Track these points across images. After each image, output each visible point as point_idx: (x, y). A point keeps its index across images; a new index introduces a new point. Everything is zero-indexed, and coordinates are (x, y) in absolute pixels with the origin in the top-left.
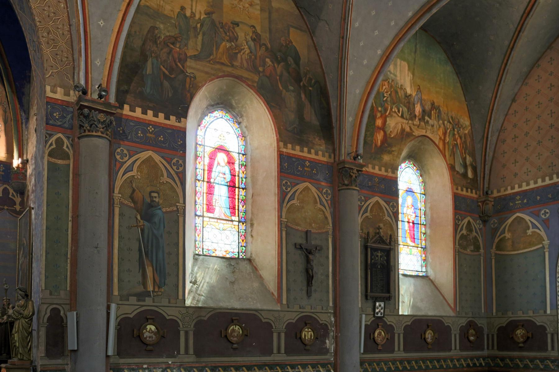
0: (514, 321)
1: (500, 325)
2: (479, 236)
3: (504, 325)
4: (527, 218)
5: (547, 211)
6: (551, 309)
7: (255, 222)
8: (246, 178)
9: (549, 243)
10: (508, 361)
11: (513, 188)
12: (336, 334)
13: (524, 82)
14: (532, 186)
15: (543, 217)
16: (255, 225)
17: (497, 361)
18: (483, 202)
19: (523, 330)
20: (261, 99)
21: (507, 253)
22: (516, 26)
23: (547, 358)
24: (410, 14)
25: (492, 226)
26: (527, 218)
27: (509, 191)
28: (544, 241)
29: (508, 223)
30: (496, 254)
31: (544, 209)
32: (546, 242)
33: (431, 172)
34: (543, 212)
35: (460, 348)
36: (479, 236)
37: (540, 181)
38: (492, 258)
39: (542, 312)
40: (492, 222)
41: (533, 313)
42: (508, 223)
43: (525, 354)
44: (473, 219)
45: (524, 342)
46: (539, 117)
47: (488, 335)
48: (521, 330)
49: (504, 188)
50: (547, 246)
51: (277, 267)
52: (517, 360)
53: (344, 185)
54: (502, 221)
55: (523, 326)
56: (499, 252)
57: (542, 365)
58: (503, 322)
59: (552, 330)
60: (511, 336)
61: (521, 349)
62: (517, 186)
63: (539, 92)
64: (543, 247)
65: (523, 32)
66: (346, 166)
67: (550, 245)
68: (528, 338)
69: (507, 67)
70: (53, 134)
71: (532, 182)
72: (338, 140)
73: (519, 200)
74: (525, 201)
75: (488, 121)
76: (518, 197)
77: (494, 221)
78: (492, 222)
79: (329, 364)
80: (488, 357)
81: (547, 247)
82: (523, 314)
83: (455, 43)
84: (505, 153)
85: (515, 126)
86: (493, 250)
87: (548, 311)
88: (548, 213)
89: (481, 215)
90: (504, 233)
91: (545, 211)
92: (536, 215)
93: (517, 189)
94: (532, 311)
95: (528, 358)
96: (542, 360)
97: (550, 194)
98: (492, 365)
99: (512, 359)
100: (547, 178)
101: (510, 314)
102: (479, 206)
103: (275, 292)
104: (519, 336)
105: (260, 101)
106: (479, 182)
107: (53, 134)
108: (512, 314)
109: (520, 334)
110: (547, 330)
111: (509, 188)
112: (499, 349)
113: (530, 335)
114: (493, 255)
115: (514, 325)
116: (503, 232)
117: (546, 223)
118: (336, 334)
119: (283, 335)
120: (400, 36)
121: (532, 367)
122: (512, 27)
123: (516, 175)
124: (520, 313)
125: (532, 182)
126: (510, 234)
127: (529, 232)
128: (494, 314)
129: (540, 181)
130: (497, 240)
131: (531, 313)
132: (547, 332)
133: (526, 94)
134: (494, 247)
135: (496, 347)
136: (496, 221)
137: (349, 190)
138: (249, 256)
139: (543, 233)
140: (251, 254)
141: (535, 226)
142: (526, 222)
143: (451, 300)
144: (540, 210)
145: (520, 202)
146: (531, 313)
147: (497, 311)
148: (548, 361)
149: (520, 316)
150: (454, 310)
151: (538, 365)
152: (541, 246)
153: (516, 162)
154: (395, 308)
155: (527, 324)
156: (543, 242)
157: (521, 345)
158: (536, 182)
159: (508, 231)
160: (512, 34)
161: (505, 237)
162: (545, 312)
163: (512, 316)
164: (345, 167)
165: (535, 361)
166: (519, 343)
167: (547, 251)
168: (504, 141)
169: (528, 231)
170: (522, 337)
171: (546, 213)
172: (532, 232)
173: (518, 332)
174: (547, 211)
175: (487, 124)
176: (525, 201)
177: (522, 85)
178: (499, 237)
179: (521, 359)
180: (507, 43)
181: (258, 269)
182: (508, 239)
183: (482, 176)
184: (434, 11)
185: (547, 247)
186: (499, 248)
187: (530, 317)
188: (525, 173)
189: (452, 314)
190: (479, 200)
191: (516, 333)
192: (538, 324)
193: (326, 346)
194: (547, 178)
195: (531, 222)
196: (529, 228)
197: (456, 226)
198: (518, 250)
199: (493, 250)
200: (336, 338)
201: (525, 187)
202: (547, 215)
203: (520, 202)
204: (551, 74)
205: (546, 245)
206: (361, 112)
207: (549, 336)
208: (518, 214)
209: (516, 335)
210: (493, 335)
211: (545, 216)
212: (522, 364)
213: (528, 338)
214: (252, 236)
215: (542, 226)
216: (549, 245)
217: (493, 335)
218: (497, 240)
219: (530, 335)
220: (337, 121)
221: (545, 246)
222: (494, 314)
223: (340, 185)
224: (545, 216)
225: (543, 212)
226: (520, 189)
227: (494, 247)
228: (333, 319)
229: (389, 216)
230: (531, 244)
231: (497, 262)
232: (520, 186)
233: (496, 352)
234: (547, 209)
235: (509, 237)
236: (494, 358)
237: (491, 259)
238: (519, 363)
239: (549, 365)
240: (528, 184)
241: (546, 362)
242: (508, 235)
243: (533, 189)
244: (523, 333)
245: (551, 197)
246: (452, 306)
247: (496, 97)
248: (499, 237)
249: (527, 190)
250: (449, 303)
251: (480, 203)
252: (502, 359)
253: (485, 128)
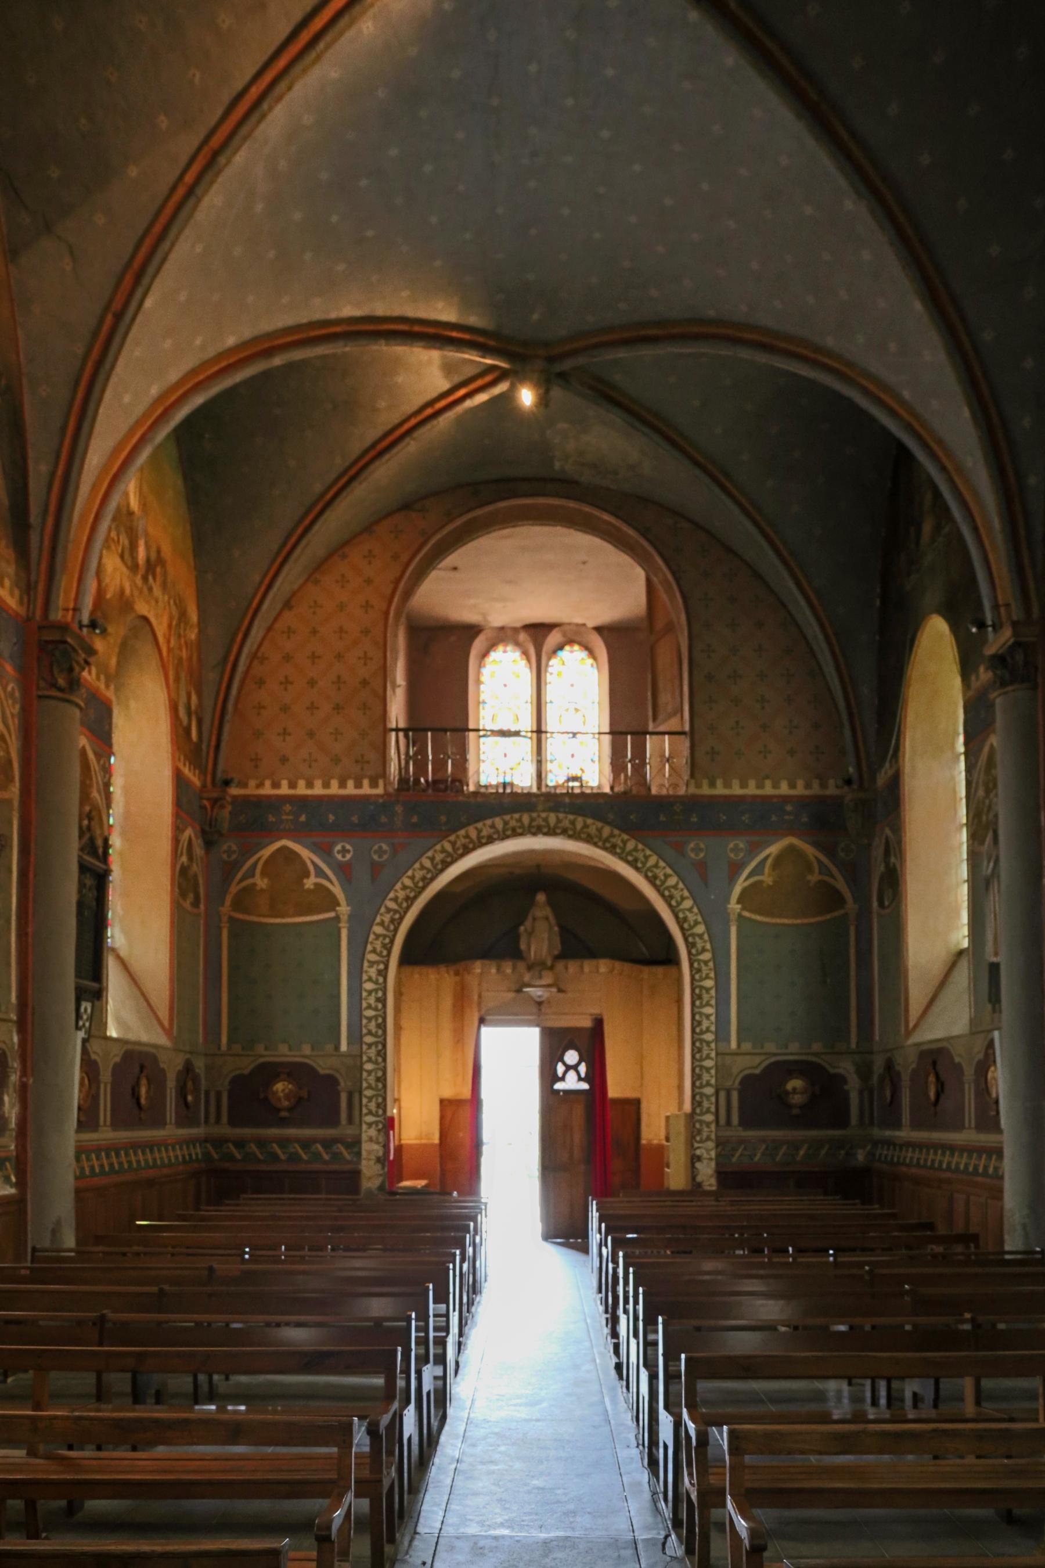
0: (269, 1063)
1: (238, 1072)
3: (246, 1072)
4: (305, 853)
5: (348, 847)
6: (349, 1044)
9: (349, 912)
10: (253, 1147)
11: (276, 785)
13: (310, 575)
14: (318, 790)
15: (339, 857)
17: (228, 1148)
18: (215, 802)
19: (290, 1083)
21: (255, 919)
22: (347, 464)
24: (231, 341)
25: (225, 856)
26: (305, 853)
27: (267, 790)
28: (339, 905)
29: (259, 859)
30: (232, 920)
31: (343, 841)
32: (344, 909)
33: (133, 704)
34: (339, 847)
37: (334, 783)
38: (223, 925)
39: (329, 1047)
40: (225, 847)
41: (313, 1049)
42: (259, 859)
43: (292, 1132)
44: (732, 879)
45: (290, 1109)
46: (339, 657)
47: (207, 1093)
48: (286, 1083)
49: (257, 782)
52: (274, 1145)
53: (54, 685)
54: (249, 850)
55: (289, 1074)
56: (241, 916)
57: (327, 1153)
58: (246, 1065)
59: (349, 1084)
60: (262, 1096)
61: (283, 1123)
62: (285, 783)
63: (341, 607)
64: (337, 919)
65: (360, 484)
66: (69, 640)
67: (351, 917)
68: (300, 1099)
69: (309, 536)
71: (318, 783)
72: (44, 566)
73: (288, 814)
74: (303, 818)
75: (244, 628)
76: (288, 807)
77: (229, 846)
78: (225, 847)
79: (7, 1159)
80: (206, 1141)
81: (344, 918)
82: (290, 1049)
83: (207, 436)
84: (261, 707)
85: (287, 658)
86: (226, 909)
87: (344, 1047)
88: (348, 851)
89: (207, 829)
90: (253, 876)
91: (343, 847)
92: (324, 851)
93: (284, 790)
94: (309, 1045)
95: (298, 1140)
96: (328, 1144)
97: (356, 816)
98: (216, 1156)
99: (262, 1143)
100: (350, 783)
101: (260, 1049)
102: (203, 808)
104: (281, 1095)
106: (204, 754)
108: (266, 1049)
109: (283, 1090)
111: (268, 783)
112: (233, 1122)
113: (305, 1095)
114: (225, 919)
115: (270, 1072)
116: (251, 873)
117: (344, 871)
120: (201, 377)
121: (305, 1157)
122: (339, 463)
123: (284, 760)
124: (283, 1049)
125: (318, 783)
127: (309, 883)
129: (334, 783)
130: (234, 889)
131: (307, 1050)
133: (315, 602)
135: (225, 1119)
136: (234, 848)
137: (66, 705)
139: (337, 890)
141: (320, 873)
142: (303, 863)
143: (164, 1013)
144: (334, 844)
145: (291, 817)
146: (307, 1050)
147: (230, 1041)
148: (339, 1145)
149: (284, 1054)
150: (168, 1032)
151: (320, 1154)
152: (332, 914)
153: (285, 733)
154: (102, 1021)
155: (298, 1072)
156: (338, 908)
157: (284, 1114)
160: (333, 476)
161: (254, 885)
162: (337, 1047)
164: (65, 642)
166: (279, 1110)
167: (344, 927)
168: (261, 682)
169: (305, 881)
170: (287, 1097)
171: (344, 851)
172: (316, 884)
173: (279, 1086)
174: (348, 847)
175: (240, 636)
176: (303, 818)
177: (307, 580)
179: (283, 1142)
180: (318, 488)
182: (262, 890)
183: (213, 743)
184: (277, 361)
185: (344, 918)
186: (238, 904)
188: (305, 760)
189: (163, 1040)
190: (205, 795)
191: (275, 1088)
192: (322, 1072)
193: (4, 1112)
194: (350, 783)
195: (313, 862)
196: (307, 874)
197: (176, 841)
198: (283, 917)
199: (226, 909)
200: (23, 1090)
201: (302, 790)
202: (348, 856)
203: (291, 817)
204: (369, 581)
205: (344, 915)
206: (92, 516)
207: (344, 1097)
209: (275, 1093)
210: (219, 1095)
211: (344, 856)
212: (284, 1153)
213: (300, 1099)
215: (335, 874)
216: (350, 916)
217: (219, 1095)
219: (305, 1095)
220: (45, 511)
221: (341, 916)
223: (42, 684)
224: (344, 856)
225: (339, 847)
226: (292, 792)
228: (16, 1039)
229: (99, 792)
231: (232, 936)
232: (293, 785)
233: (225, 1130)
234: (348, 843)
236: (219, 1142)
237: (220, 928)
238: (300, 1151)
239: (341, 1153)
240: (310, 785)
241: (335, 1147)
242: (261, 883)
244: (291, 1091)
245: (356, 821)
246: (166, 1023)
247: (270, 587)
250: (162, 1018)
251: (206, 803)
252: (240, 1144)
253: (232, 641)
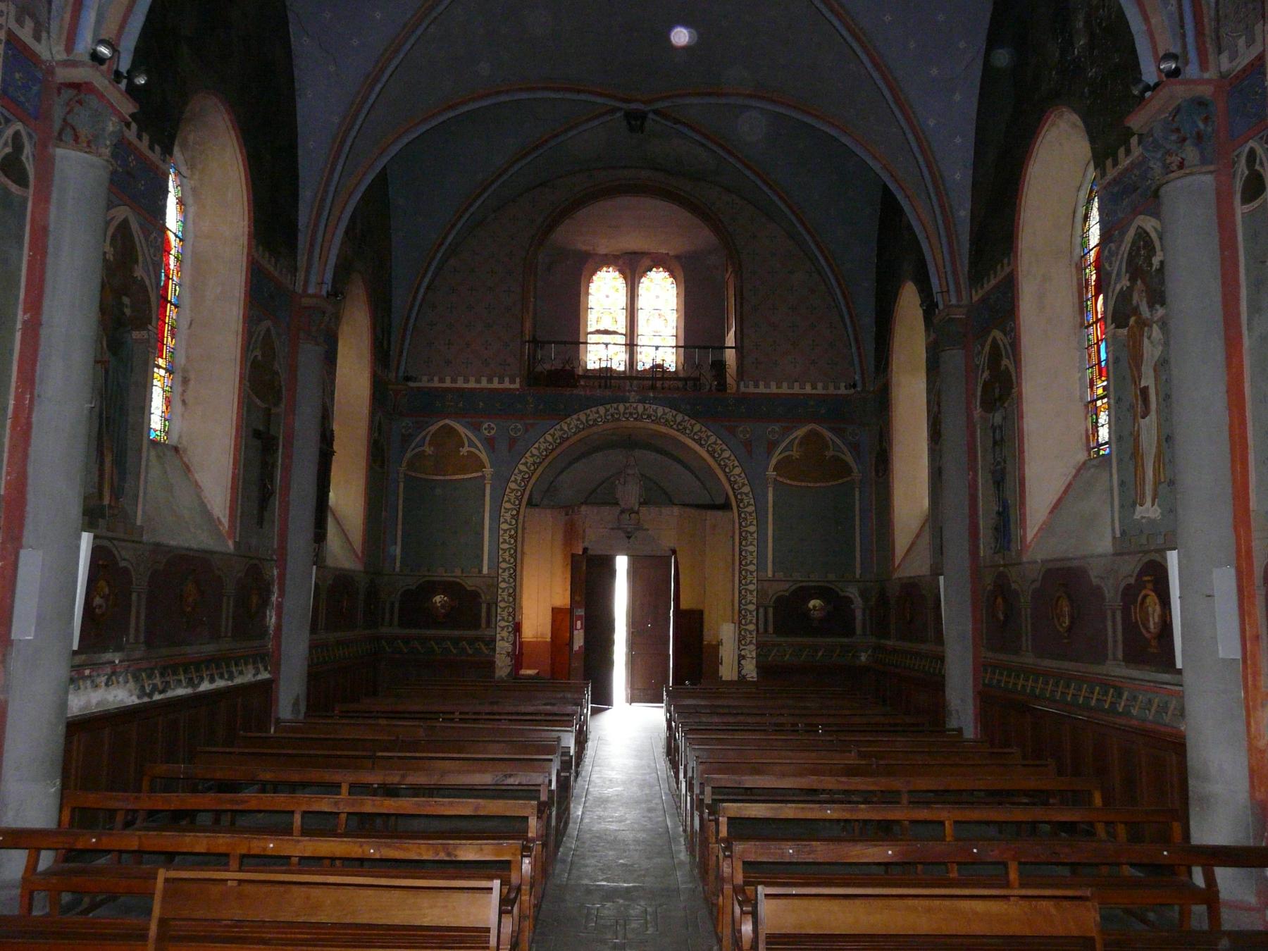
2: (479, 450)
5: (493, 425)
7: (192, 376)
8: (180, 285)
11: (442, 380)
12: (280, 600)
15: (486, 432)
16: (192, 383)
20: (241, 153)
23: (477, 639)
34: (486, 426)
35: (775, 628)
36: (479, 450)
37: (484, 380)
41: (462, 572)
43: (446, 632)
50: (490, 476)
51: (230, 472)
64: (483, 477)
70: (1013, 270)
71: (472, 379)
81: (488, 477)
87: (485, 571)
92: (476, 428)
96: (472, 641)
100: (496, 380)
103: (224, 517)
105: (239, 156)
107: (1013, 270)
110: (480, 597)
117: (490, 443)
118: (280, 600)
119: (771, 611)
126: (432, 448)
128: (397, 569)
130: (408, 455)
132: (853, 606)
134: (404, 464)
138: (174, 440)
139: (484, 456)
140: (180, 437)
141: (471, 444)
146: (458, 572)
148: (480, 643)
152: (480, 474)
155: (452, 588)
158: (478, 381)
159: (429, 444)
162: (480, 571)
163: (426, 574)
165: (461, 644)
171: (490, 428)
178: (413, 449)
181: (192, 468)
185: (488, 477)
187: (455, 577)
194: (496, 380)
201: (460, 384)
207: (484, 607)
208: (447, 421)
214: (184, 402)
218: (408, 455)
222: (397, 569)
225: (486, 426)
227: (404, 464)
230: (464, 470)
232: (454, 381)
235: (431, 453)
243: (471, 389)
248: (413, 449)
249: (475, 389)
